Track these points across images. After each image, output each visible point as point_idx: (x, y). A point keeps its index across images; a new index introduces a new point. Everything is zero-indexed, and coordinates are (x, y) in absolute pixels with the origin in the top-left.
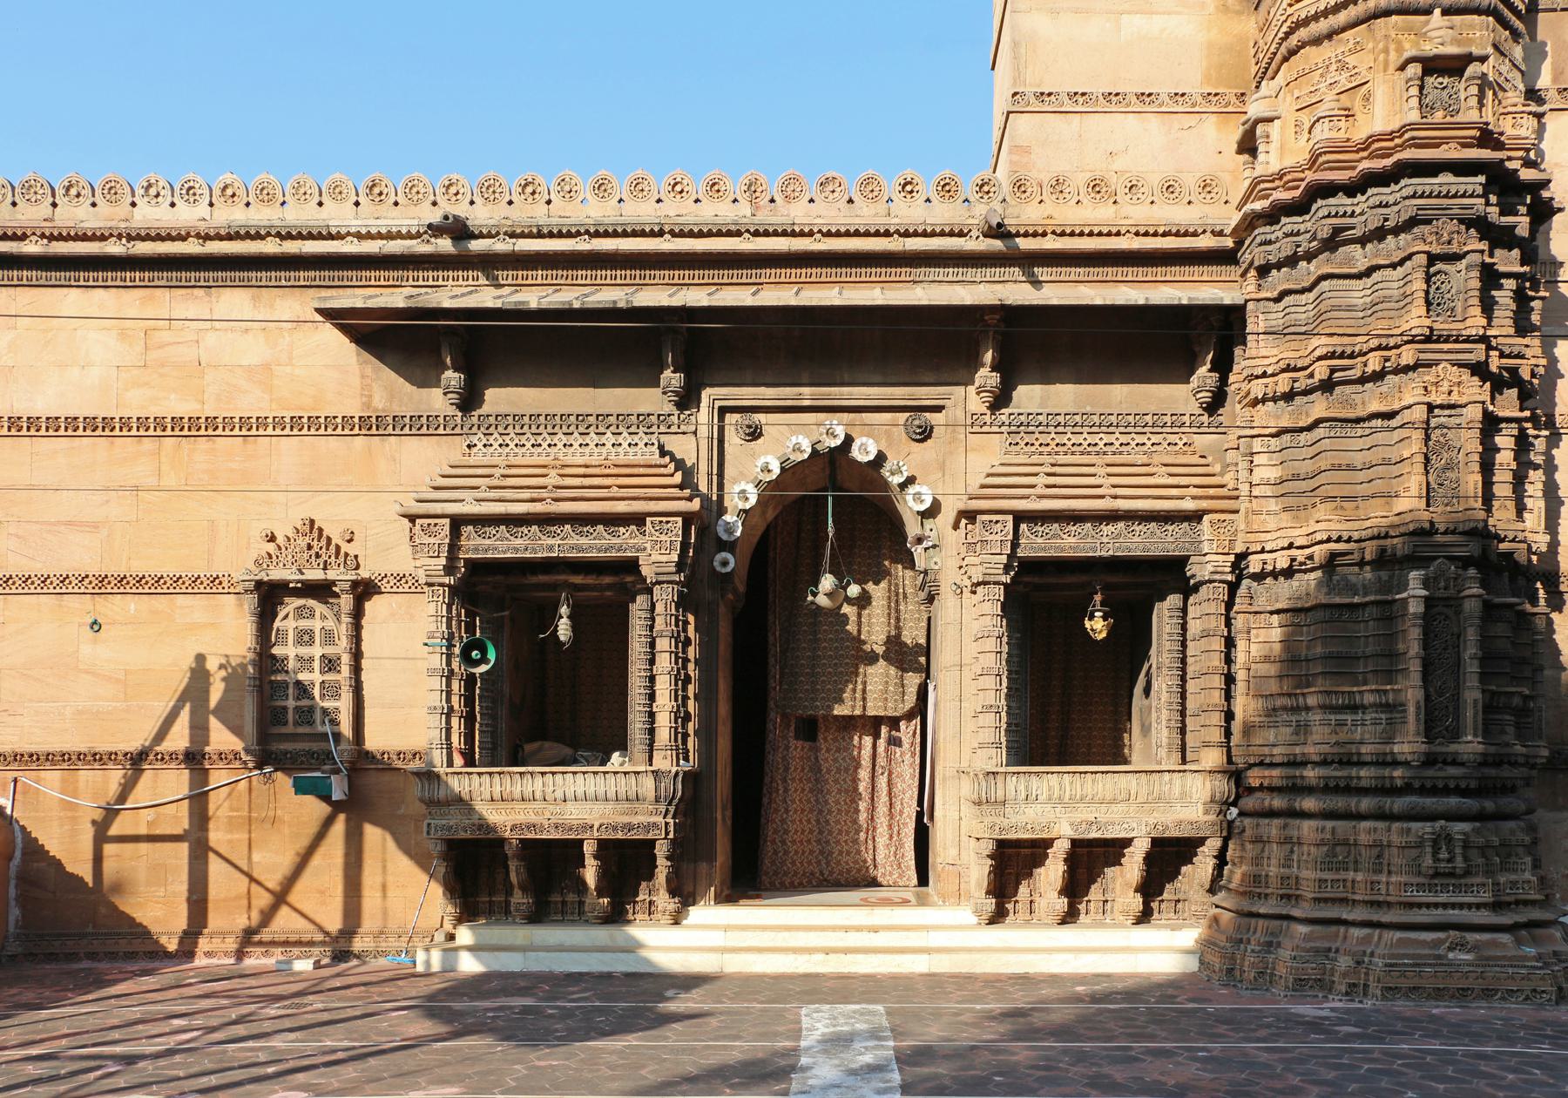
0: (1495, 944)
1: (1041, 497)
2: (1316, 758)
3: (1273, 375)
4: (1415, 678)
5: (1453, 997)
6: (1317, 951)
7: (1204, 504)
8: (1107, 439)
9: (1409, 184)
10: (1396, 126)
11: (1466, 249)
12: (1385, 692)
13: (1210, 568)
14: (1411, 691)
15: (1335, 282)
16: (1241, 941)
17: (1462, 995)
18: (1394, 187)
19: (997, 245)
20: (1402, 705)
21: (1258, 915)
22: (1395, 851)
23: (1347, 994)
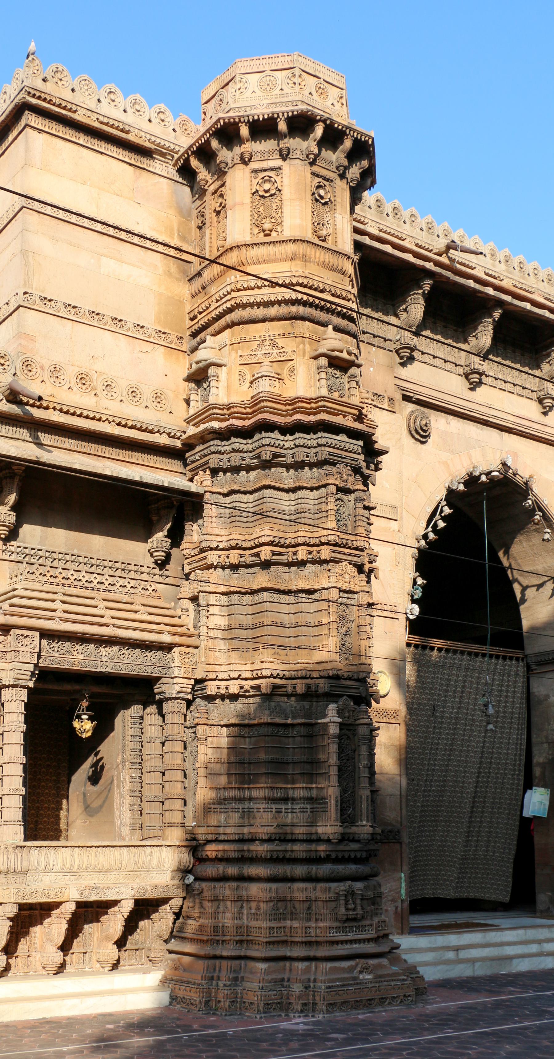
0: (380, 966)
1: (62, 620)
2: (265, 837)
3: (222, 550)
4: (334, 780)
5: (364, 1006)
6: (275, 981)
7: (177, 639)
8: (99, 578)
9: (324, 437)
10: (314, 396)
11: (356, 487)
12: (311, 789)
13: (177, 688)
14: (331, 790)
15: (272, 491)
16: (212, 978)
17: (369, 1004)
18: (312, 436)
19: (14, 409)
20: (323, 798)
21: (221, 957)
22: (320, 904)
23: (302, 1011)
